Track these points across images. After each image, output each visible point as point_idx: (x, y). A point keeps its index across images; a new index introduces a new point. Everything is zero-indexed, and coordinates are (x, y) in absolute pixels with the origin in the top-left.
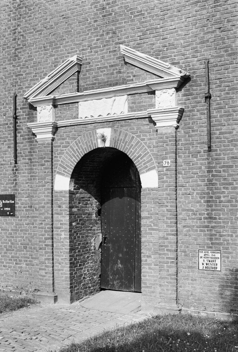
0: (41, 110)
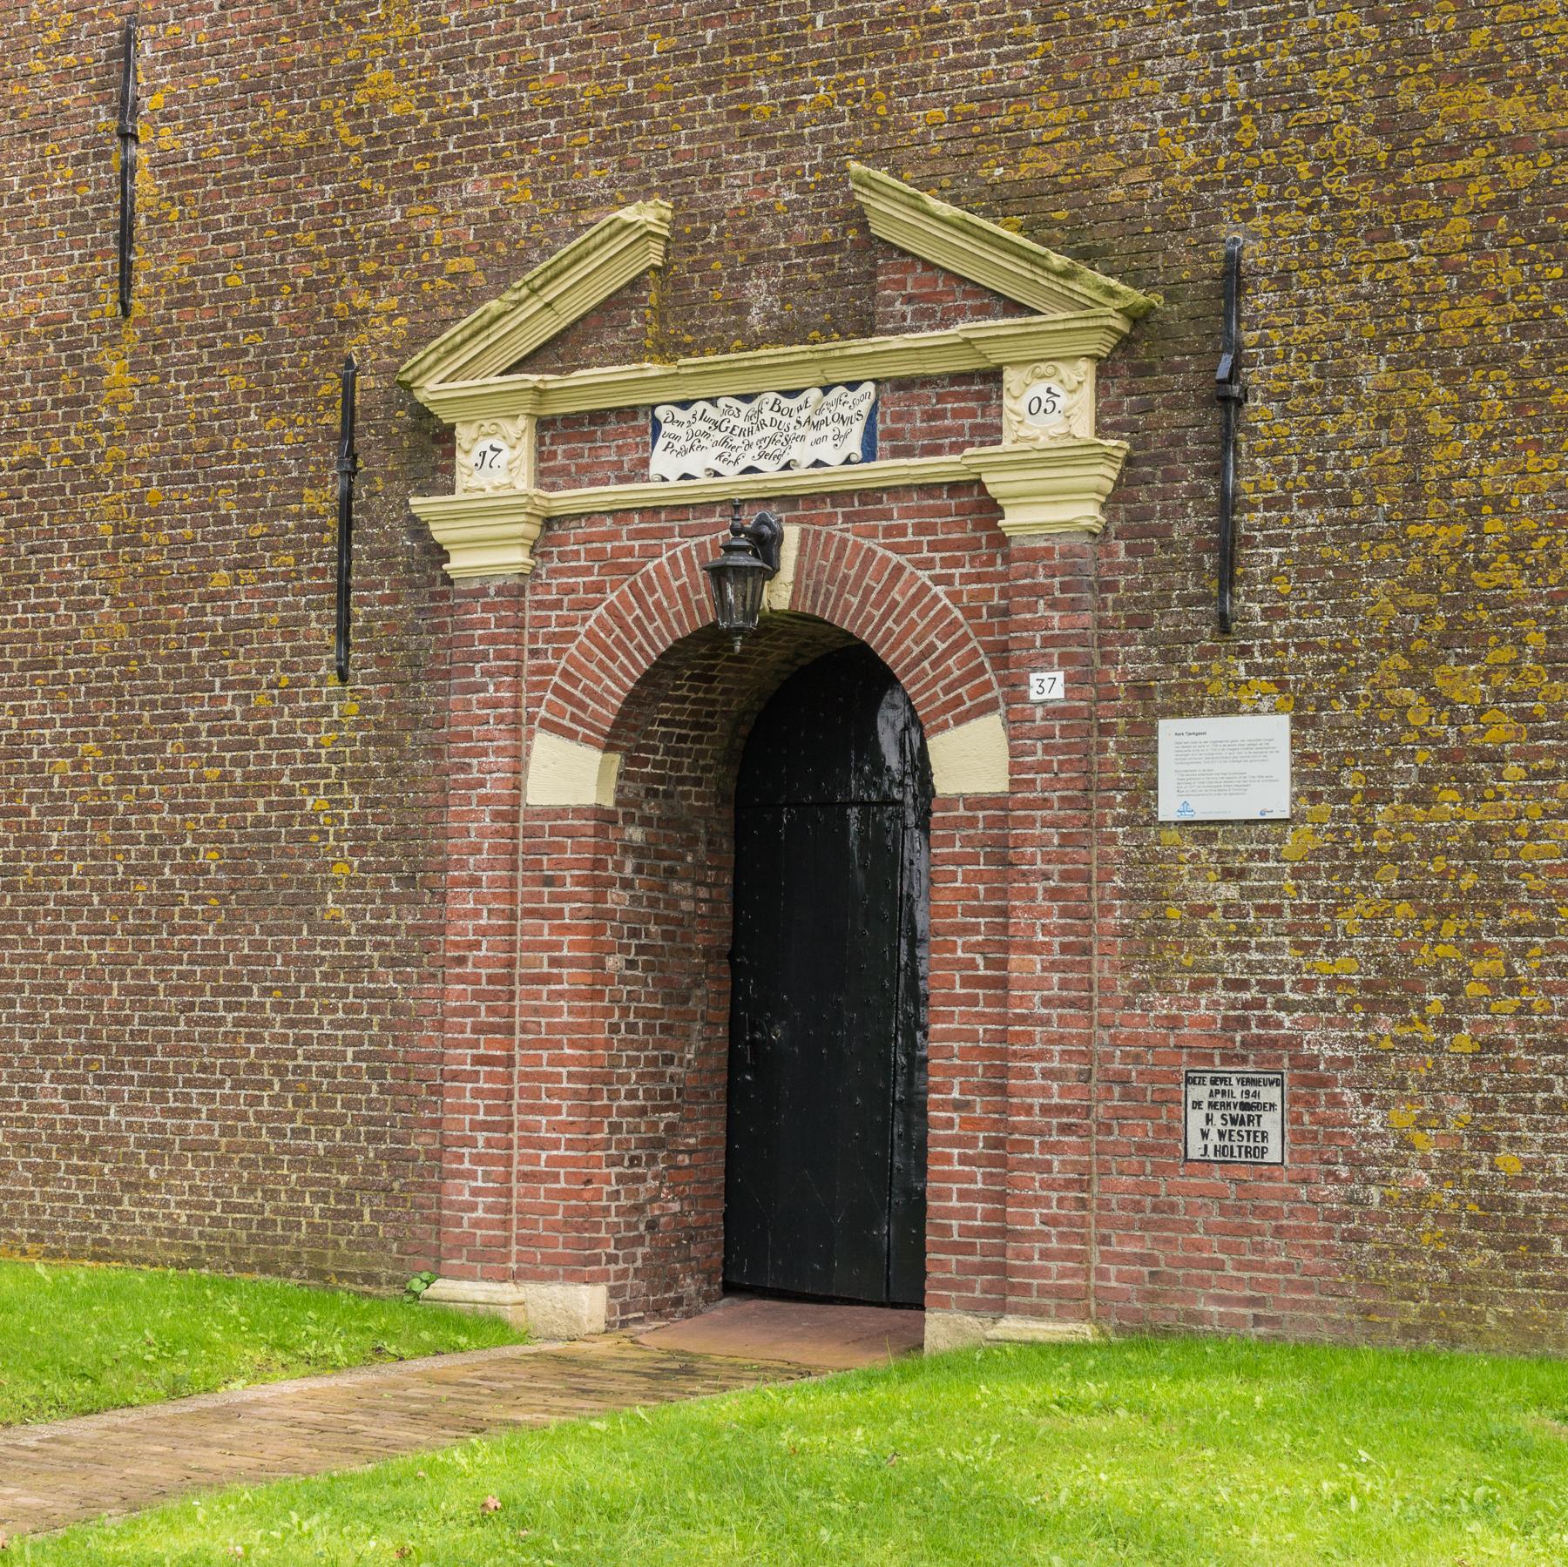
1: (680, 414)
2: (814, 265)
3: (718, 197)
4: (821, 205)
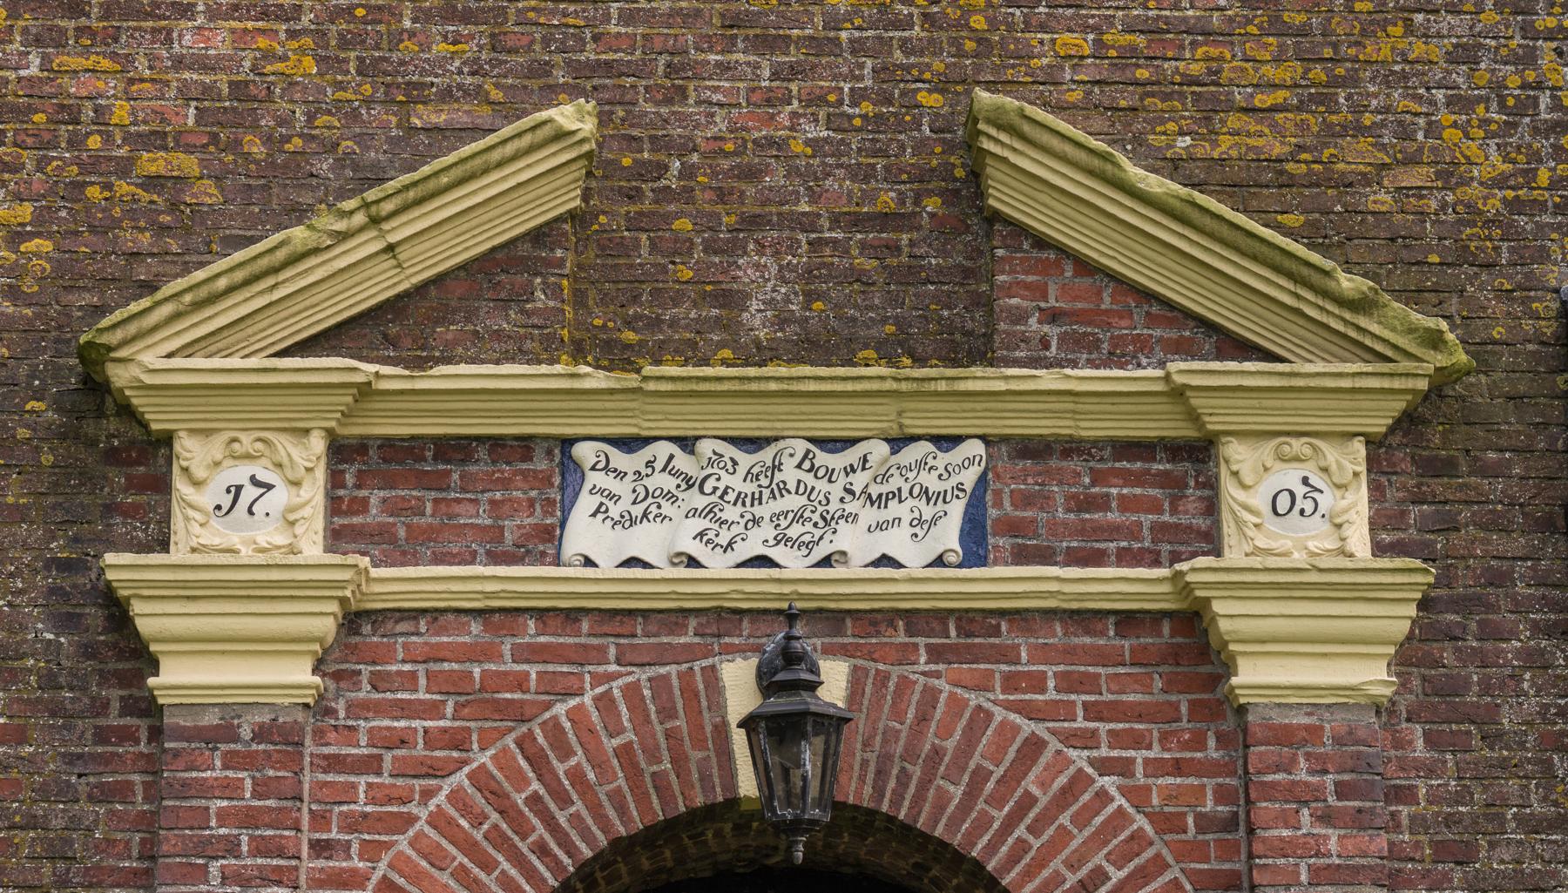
0: (217, 464)
1: (619, 459)
2: (863, 245)
3: (682, 118)
4: (875, 154)
